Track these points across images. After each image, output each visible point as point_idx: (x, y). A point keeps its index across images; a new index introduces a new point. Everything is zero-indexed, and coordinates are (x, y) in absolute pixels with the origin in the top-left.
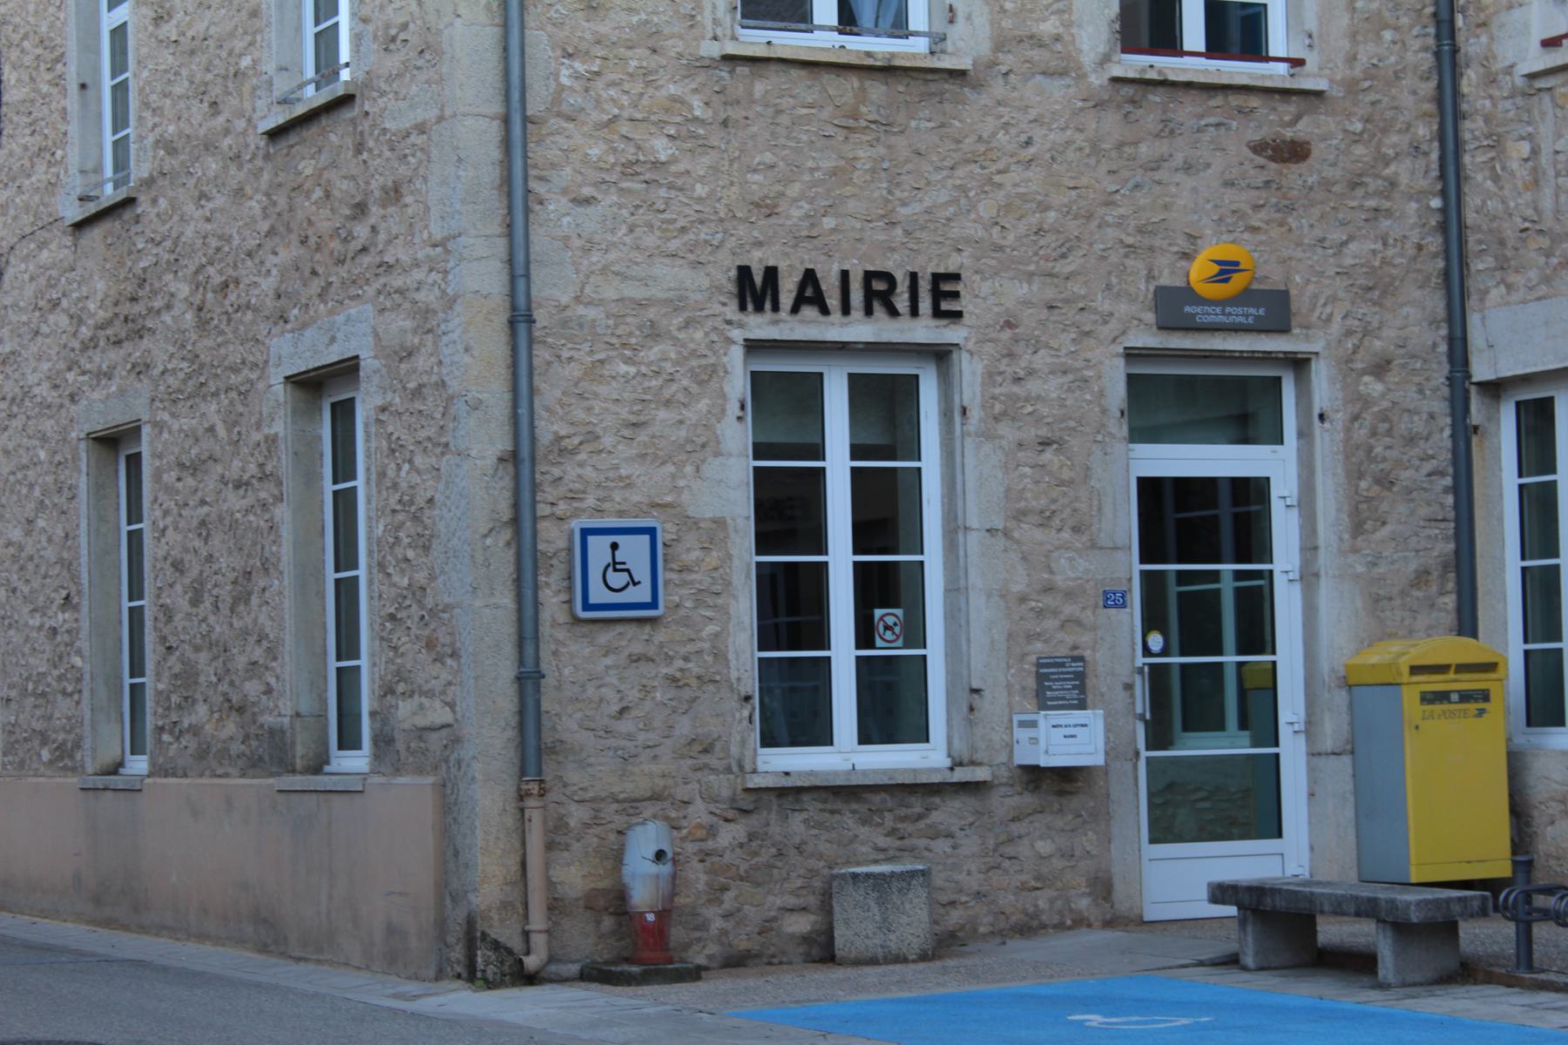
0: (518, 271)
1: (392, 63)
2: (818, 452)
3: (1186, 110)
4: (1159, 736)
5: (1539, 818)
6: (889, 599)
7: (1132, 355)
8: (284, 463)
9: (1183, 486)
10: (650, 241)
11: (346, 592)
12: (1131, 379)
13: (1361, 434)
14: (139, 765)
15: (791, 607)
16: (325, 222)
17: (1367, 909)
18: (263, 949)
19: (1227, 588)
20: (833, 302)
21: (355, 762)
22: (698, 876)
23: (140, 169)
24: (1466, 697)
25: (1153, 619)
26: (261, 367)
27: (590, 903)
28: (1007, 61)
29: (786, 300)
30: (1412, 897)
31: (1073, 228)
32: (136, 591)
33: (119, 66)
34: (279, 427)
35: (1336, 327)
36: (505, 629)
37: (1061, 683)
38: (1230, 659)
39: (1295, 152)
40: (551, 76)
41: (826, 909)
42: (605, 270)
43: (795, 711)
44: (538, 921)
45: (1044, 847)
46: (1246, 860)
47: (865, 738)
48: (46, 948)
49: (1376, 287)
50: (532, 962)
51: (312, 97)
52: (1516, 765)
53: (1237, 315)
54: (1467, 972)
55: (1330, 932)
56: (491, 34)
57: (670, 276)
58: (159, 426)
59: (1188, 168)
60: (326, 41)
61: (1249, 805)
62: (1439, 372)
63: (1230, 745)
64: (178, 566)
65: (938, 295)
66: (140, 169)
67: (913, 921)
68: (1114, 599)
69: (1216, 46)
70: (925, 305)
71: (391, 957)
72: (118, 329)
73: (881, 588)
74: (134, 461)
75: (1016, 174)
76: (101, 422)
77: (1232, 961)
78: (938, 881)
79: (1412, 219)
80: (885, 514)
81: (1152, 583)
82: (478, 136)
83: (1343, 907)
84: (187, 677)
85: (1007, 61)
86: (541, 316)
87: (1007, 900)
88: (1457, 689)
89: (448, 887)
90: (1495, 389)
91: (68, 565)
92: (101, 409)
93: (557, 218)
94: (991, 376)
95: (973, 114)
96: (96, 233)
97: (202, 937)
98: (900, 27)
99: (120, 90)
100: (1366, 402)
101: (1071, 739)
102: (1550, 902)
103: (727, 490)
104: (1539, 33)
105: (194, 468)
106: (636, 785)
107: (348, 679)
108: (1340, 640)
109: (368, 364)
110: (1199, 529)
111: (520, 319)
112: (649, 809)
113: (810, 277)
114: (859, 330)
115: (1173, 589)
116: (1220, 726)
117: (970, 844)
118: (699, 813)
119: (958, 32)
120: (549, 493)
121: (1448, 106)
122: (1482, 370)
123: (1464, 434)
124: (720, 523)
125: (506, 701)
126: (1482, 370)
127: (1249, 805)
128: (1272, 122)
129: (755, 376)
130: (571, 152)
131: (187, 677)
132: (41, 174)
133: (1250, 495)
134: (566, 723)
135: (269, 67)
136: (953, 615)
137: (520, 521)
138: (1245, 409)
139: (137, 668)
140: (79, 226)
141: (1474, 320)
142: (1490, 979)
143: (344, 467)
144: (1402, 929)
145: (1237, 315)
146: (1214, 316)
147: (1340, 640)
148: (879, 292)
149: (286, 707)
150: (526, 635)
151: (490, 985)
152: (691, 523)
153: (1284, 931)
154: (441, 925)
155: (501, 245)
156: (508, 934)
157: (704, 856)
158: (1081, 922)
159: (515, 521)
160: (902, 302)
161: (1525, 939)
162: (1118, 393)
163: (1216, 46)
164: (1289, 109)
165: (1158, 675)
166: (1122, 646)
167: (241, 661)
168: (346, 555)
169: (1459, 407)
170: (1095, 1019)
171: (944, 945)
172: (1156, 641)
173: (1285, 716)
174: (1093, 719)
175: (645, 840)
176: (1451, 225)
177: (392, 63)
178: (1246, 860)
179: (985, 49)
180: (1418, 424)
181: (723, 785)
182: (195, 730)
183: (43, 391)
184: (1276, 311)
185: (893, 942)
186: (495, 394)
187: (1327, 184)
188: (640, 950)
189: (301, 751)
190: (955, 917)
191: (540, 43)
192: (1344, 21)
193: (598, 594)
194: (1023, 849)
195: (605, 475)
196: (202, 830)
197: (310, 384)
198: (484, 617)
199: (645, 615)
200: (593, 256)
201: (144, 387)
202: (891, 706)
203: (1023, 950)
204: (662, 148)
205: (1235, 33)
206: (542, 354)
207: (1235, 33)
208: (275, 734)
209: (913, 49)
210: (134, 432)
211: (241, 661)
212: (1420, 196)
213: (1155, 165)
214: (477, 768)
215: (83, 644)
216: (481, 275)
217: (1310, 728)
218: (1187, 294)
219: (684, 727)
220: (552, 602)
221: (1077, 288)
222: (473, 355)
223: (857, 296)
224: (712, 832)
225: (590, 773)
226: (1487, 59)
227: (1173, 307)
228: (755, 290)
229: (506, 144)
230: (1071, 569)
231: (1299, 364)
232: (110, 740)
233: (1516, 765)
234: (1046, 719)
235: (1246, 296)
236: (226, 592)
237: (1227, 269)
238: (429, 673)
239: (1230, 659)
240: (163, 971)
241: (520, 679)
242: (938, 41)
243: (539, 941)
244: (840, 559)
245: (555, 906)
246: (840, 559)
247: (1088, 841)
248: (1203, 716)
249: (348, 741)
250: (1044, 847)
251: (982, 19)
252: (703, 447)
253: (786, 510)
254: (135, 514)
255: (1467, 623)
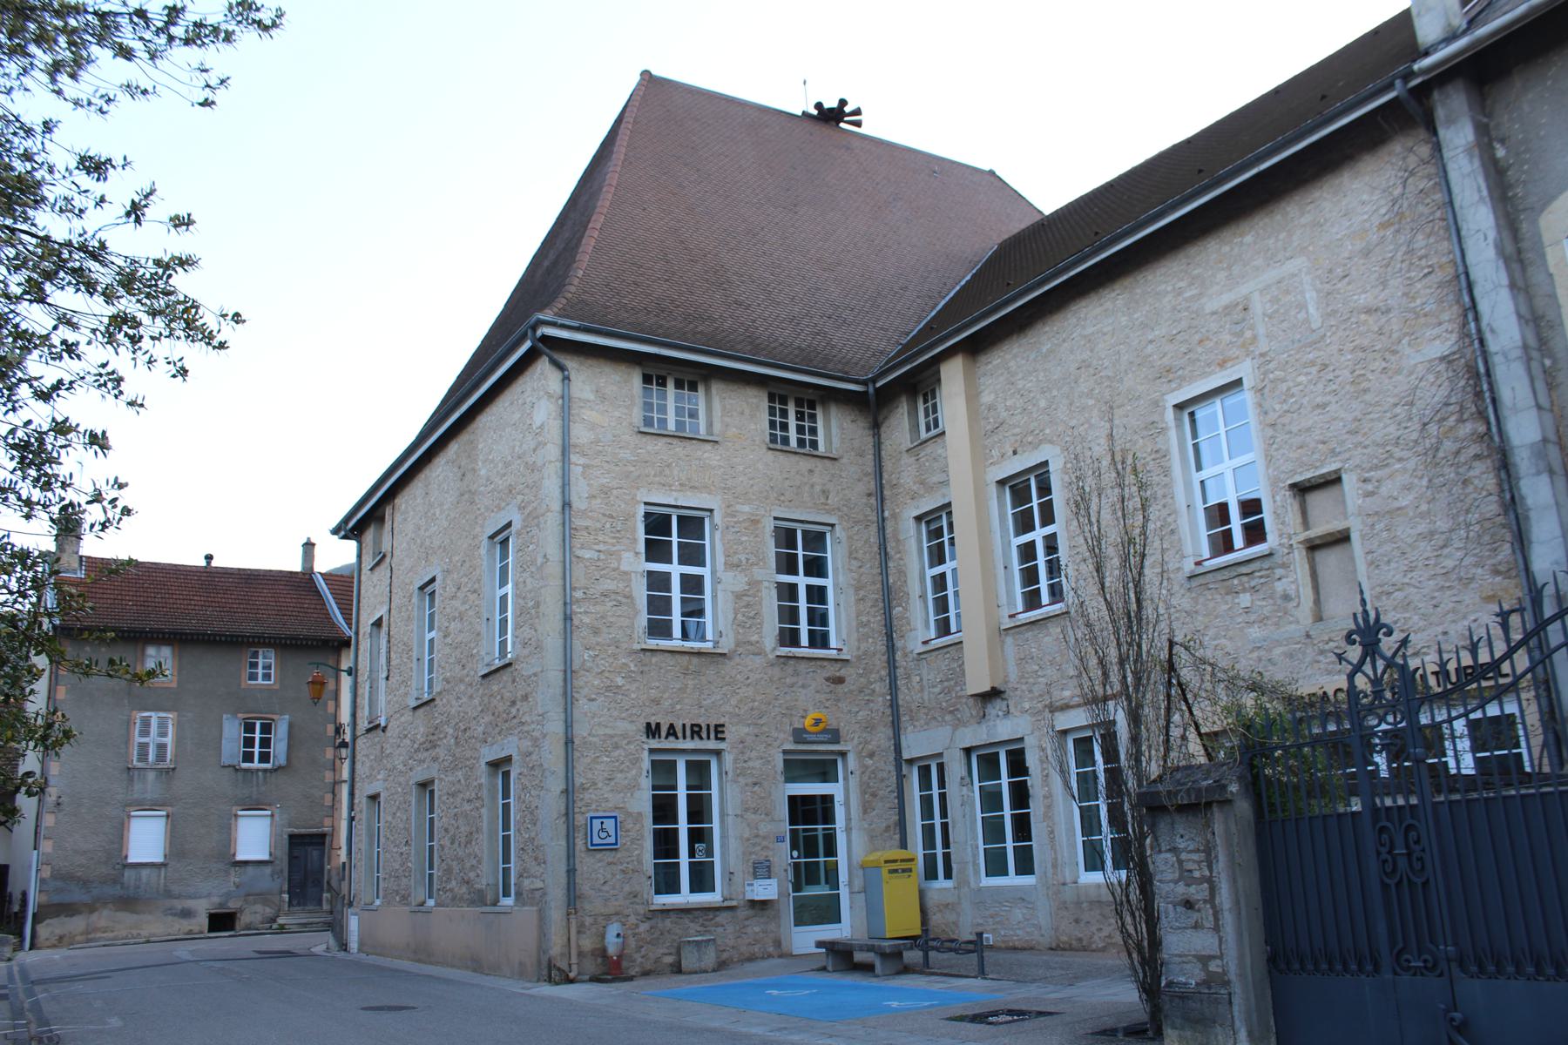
0: (569, 724)
1: (526, 652)
2: (675, 788)
3: (802, 666)
4: (797, 888)
5: (930, 913)
6: (701, 841)
7: (785, 752)
8: (485, 793)
9: (804, 797)
10: (615, 713)
11: (506, 839)
12: (785, 761)
13: (865, 778)
14: (431, 903)
15: (665, 844)
16: (501, 707)
17: (871, 949)
18: (475, 971)
19: (820, 834)
20: (680, 735)
21: (508, 902)
22: (632, 942)
23: (437, 689)
24: (904, 871)
25: (794, 846)
26: (477, 759)
27: (593, 953)
28: (740, 650)
29: (663, 734)
30: (886, 944)
31: (763, 707)
32: (431, 840)
33: (431, 652)
34: (483, 780)
35: (856, 741)
36: (563, 853)
37: (762, 869)
38: (822, 859)
39: (840, 681)
40: (581, 656)
41: (679, 953)
42: (599, 724)
43: (668, 883)
44: (574, 960)
45: (757, 929)
46: (828, 932)
47: (692, 891)
48: (397, 971)
49: (869, 727)
50: (572, 975)
51: (498, 663)
52: (922, 894)
53: (821, 737)
54: (906, 970)
55: (859, 957)
56: (561, 642)
57: (623, 726)
58: (441, 780)
59: (803, 686)
60: (503, 644)
61: (828, 912)
62: (892, 757)
63: (821, 890)
64: (446, 830)
65: (717, 732)
66: (437, 689)
67: (710, 957)
68: (780, 839)
69: (812, 644)
70: (712, 735)
71: (521, 974)
72: (427, 745)
73: (697, 836)
74: (432, 792)
75: (744, 689)
76: (421, 778)
77: (824, 969)
78: (719, 942)
79: (881, 703)
80: (699, 810)
81: (794, 833)
82: (555, 676)
83: (862, 948)
84: (449, 871)
85: (740, 650)
86: (577, 741)
87: (743, 949)
88: (901, 868)
89: (542, 947)
90: (911, 762)
91: (407, 830)
92: (420, 774)
93: (582, 706)
94: (736, 761)
95: (728, 668)
96: (421, 711)
97: (453, 966)
98: (703, 639)
99: (431, 661)
100: (867, 767)
101: (765, 890)
102: (934, 944)
103: (642, 802)
104: (921, 639)
105: (453, 795)
106: (611, 910)
107: (506, 872)
108: (860, 853)
109: (515, 758)
110: (810, 812)
111: (569, 741)
112: (615, 918)
113: (672, 726)
114: (689, 744)
115: (801, 834)
116: (818, 883)
117: (730, 929)
118: (632, 919)
119: (723, 641)
120: (579, 804)
121: (892, 665)
122: (906, 756)
123: (901, 778)
124: (640, 814)
125: (563, 880)
126: (906, 756)
127: (828, 912)
128: (832, 670)
129: (653, 762)
130: (587, 683)
131: (449, 871)
132: (402, 690)
133: (828, 800)
134: (585, 887)
135: (483, 653)
136: (723, 846)
137: (568, 814)
138: (824, 770)
139: (431, 867)
140: (415, 708)
141: (903, 738)
142: (914, 972)
143: (506, 795)
144: (884, 955)
145: (821, 737)
146: (814, 738)
147: (860, 853)
148: (696, 731)
149: (484, 882)
150: (570, 855)
151: (557, 984)
152: (629, 814)
153: (841, 957)
154: (539, 962)
155: (562, 716)
156: (563, 965)
157: (634, 935)
158: (770, 956)
159: (567, 814)
160: (704, 735)
161: (926, 957)
162: (780, 765)
163: (812, 644)
164: (838, 665)
165: (796, 866)
166: (784, 856)
167: (468, 865)
168: (506, 827)
169: (899, 768)
170: (775, 992)
171: (721, 965)
172: (795, 854)
173: (841, 879)
174: (774, 882)
175: (613, 929)
176: (894, 705)
177: (526, 652)
178: (828, 932)
179: (733, 646)
180: (885, 775)
181: (641, 909)
182: (451, 890)
183: (400, 767)
184: (835, 736)
185: (703, 965)
186: (560, 768)
187: (851, 692)
188: (611, 970)
189: (489, 898)
190: (725, 956)
191: (577, 644)
192: (855, 635)
193: (596, 840)
194: (749, 930)
195: (598, 797)
196: (454, 927)
197: (495, 765)
198: (555, 848)
199: (613, 848)
200: (594, 719)
201: (436, 765)
202: (702, 879)
203: (749, 967)
204: (620, 681)
205: (819, 639)
206: (577, 754)
207: (819, 639)
208: (480, 891)
209: (707, 646)
210: (432, 782)
211: (468, 865)
212: (883, 695)
213: (792, 686)
214: (553, 904)
215: (412, 858)
216: (556, 727)
217: (850, 884)
218: (804, 730)
219: (627, 888)
220: (580, 843)
221: (765, 729)
222: (552, 755)
223: (688, 733)
224: (637, 926)
225: (593, 905)
226: (904, 648)
227: (799, 735)
228: (652, 731)
229: (565, 680)
230: (764, 828)
231: (843, 754)
232: (420, 893)
233: (922, 894)
234: (757, 883)
235: (824, 731)
236: (463, 840)
237: (817, 722)
238: (535, 869)
239: (822, 859)
240: (438, 979)
241: (568, 871)
242: (716, 643)
243: (574, 967)
244: (683, 826)
245: (580, 954)
246: (683, 826)
247: (772, 926)
248: (812, 880)
249: (506, 894)
250: (757, 929)
251: (731, 635)
252: (634, 787)
253: (663, 809)
254: (431, 812)
255: (903, 845)
